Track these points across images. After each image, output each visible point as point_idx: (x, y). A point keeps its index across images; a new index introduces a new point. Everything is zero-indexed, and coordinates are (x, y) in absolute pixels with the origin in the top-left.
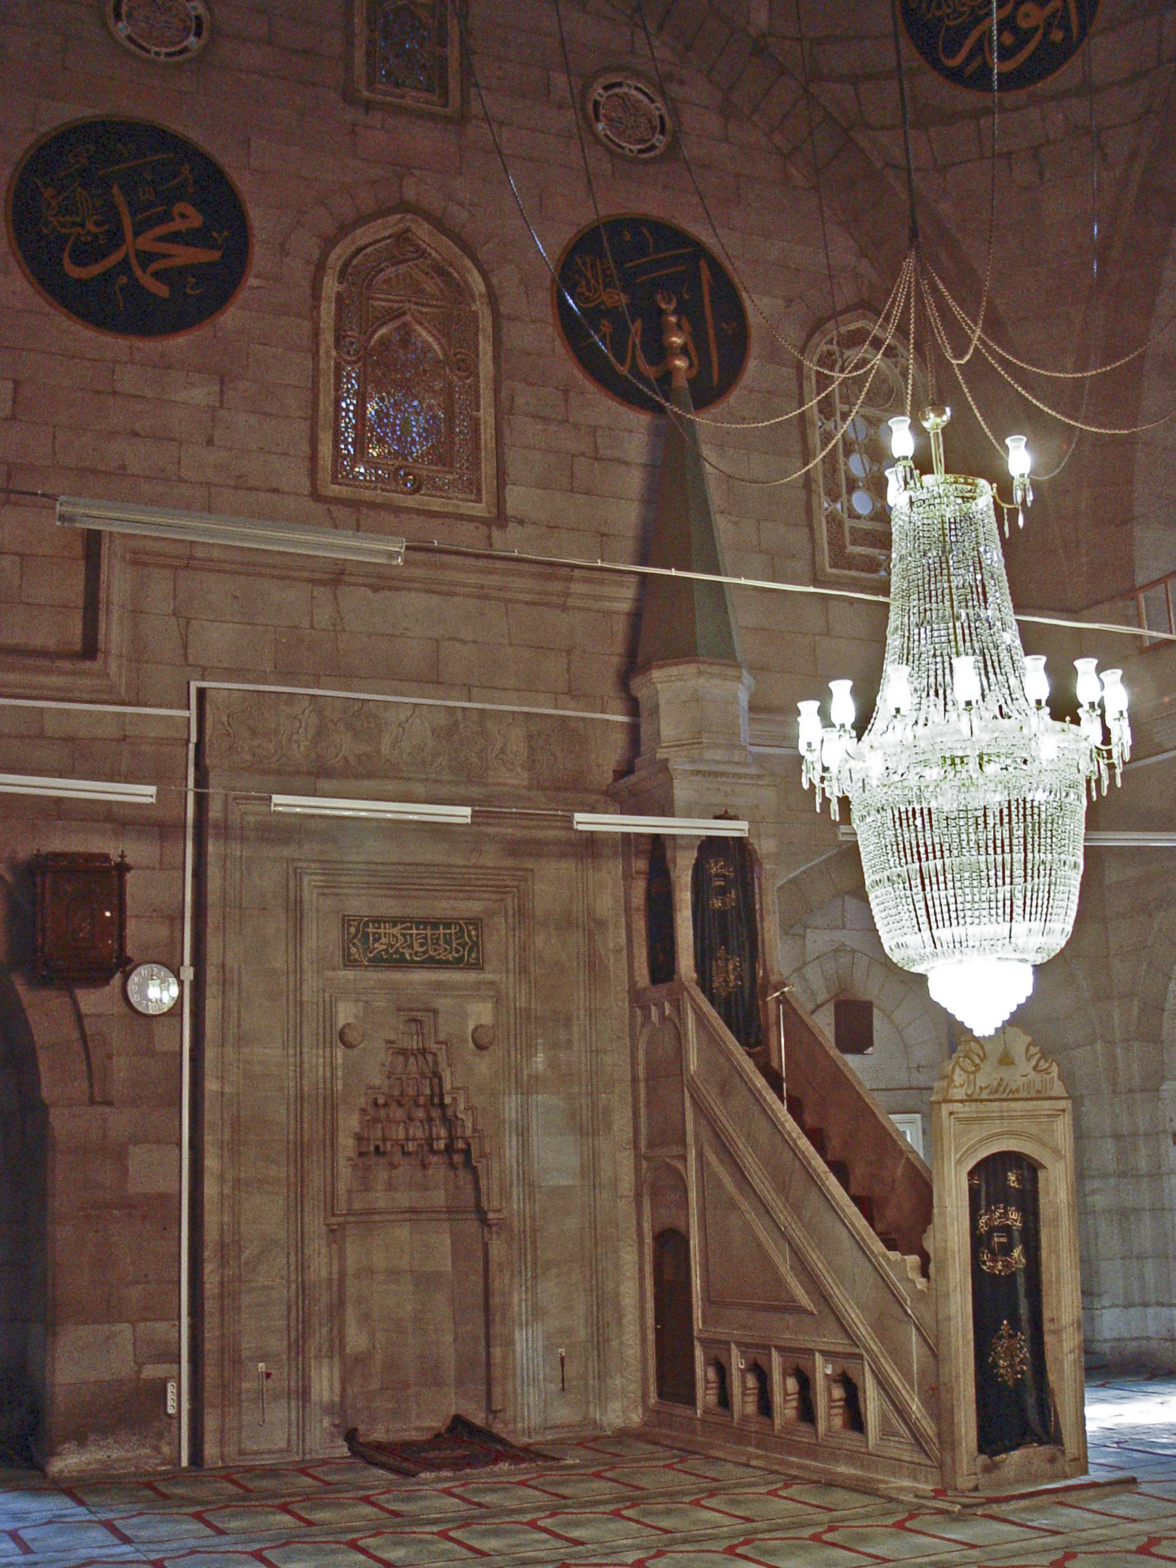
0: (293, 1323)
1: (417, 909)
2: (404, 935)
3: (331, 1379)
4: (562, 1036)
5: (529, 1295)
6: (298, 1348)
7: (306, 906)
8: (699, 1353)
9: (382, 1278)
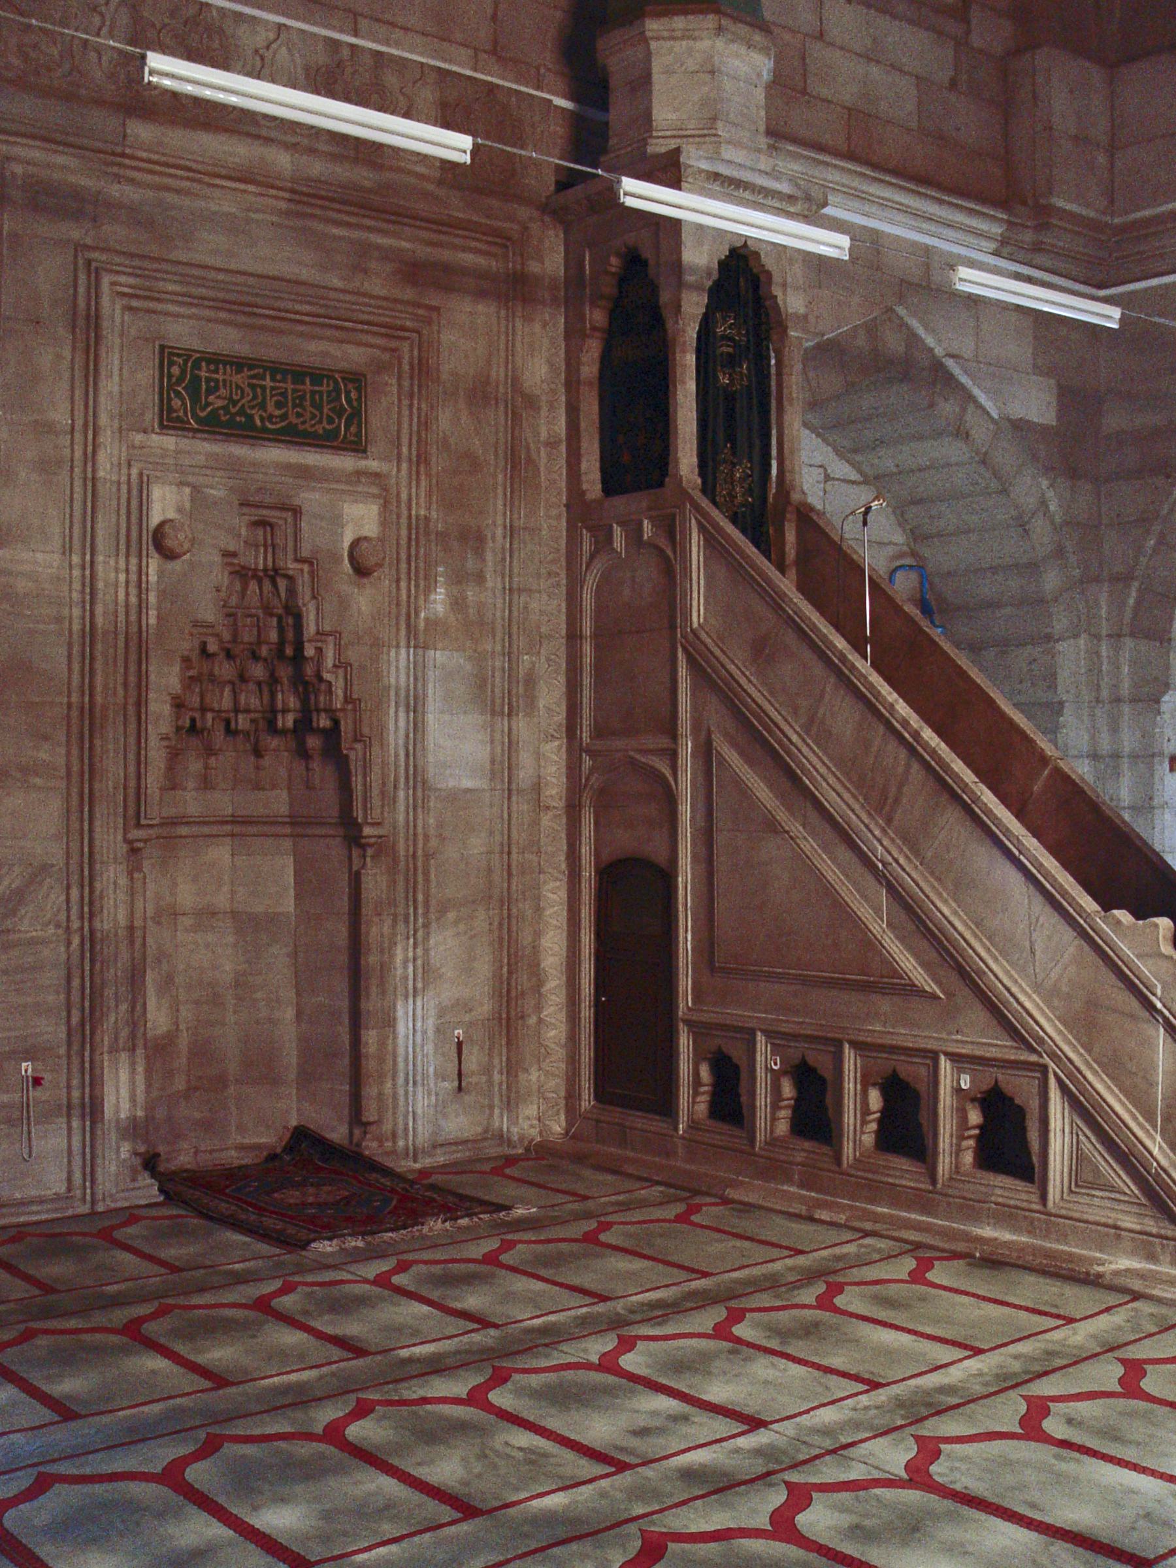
0: (75, 996)
1: (272, 348)
2: (253, 387)
3: (132, 1082)
4: (471, 564)
5: (419, 951)
6: (84, 1034)
7: (105, 324)
8: (685, 1042)
9: (191, 922)
